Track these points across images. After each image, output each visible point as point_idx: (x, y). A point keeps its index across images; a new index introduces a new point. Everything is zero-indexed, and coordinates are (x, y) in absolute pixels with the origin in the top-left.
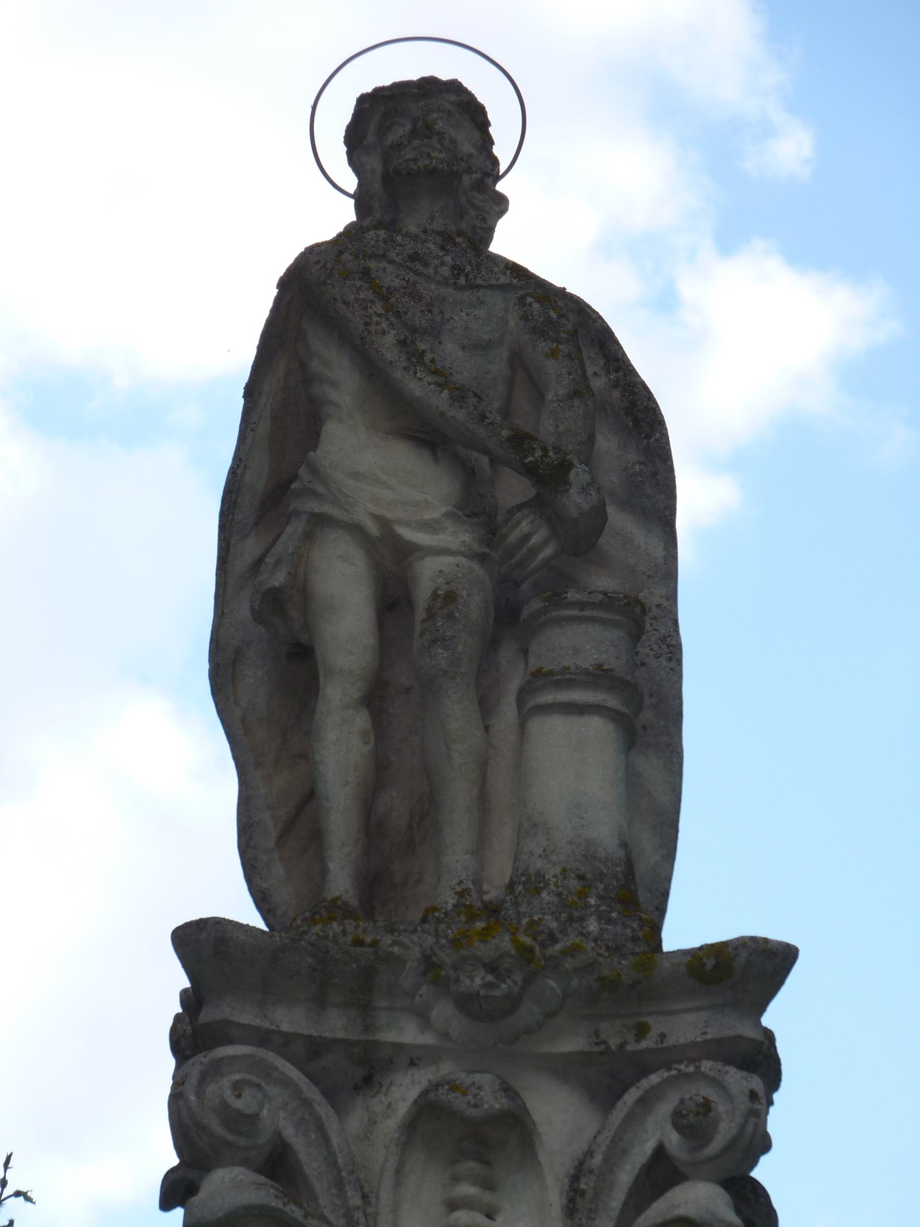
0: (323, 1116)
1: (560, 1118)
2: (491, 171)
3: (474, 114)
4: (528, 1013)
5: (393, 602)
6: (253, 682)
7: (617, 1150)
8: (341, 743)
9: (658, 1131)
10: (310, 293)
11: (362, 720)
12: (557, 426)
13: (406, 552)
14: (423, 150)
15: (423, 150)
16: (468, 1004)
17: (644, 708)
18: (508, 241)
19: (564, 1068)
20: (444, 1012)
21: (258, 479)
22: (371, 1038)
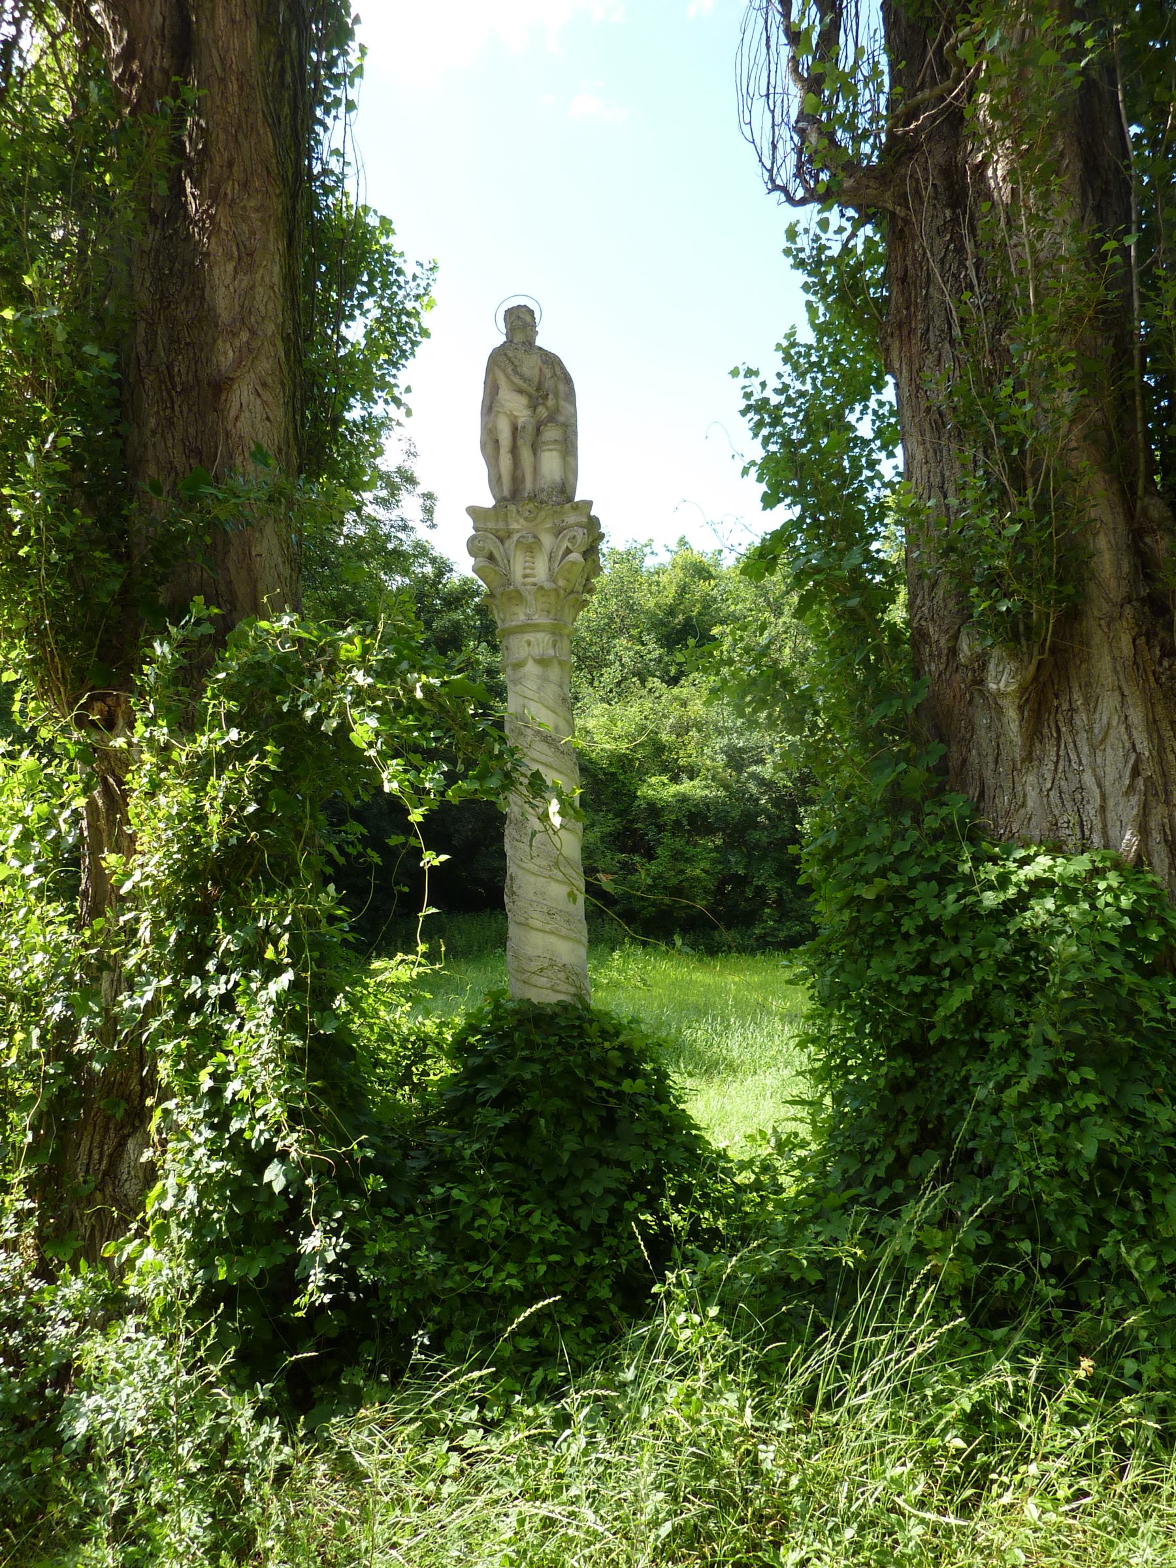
0: (791, 83)
1: (547, 540)
2: (534, 325)
3: (531, 312)
4: (539, 520)
5: (515, 430)
6: (490, 447)
7: (559, 547)
8: (505, 461)
9: (566, 544)
10: (498, 359)
11: (509, 456)
12: (366, 1551)
13: (516, 417)
14: (520, 321)
15: (520, 321)
16: (526, 519)
17: (568, 447)
18: (539, 342)
19: (547, 530)
20: (522, 521)
21: (487, 403)
22: (475, 577)
